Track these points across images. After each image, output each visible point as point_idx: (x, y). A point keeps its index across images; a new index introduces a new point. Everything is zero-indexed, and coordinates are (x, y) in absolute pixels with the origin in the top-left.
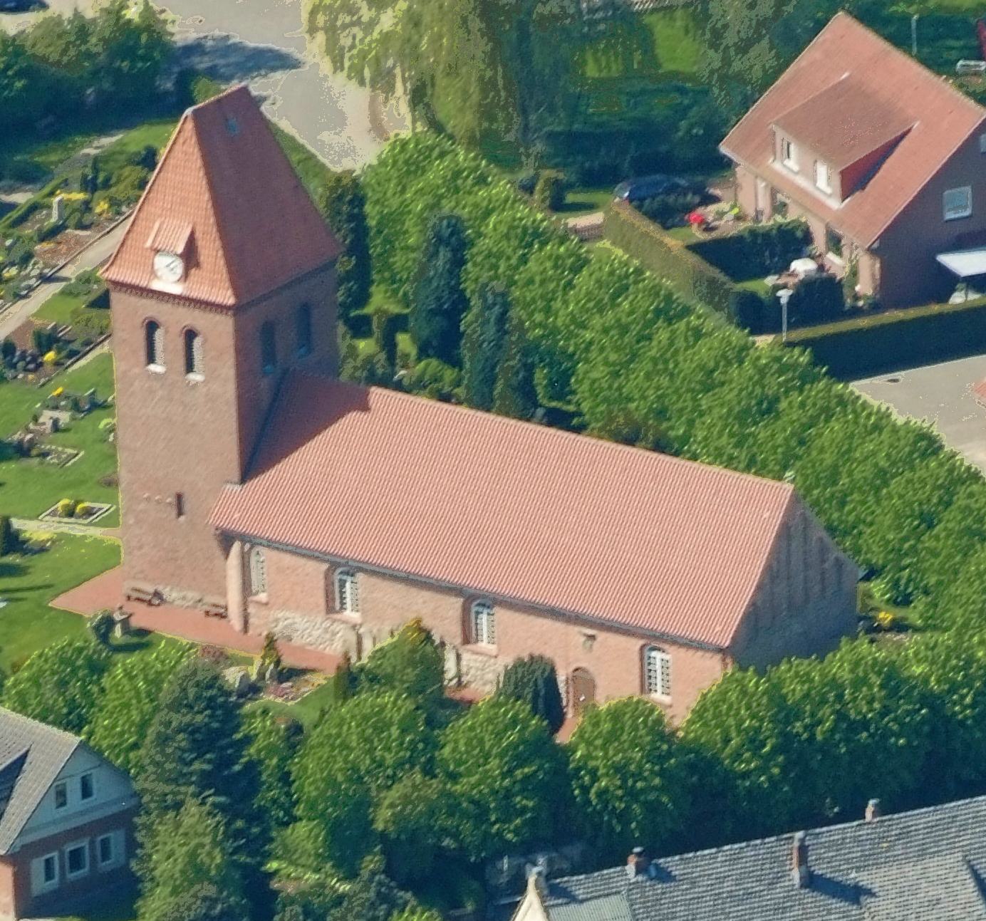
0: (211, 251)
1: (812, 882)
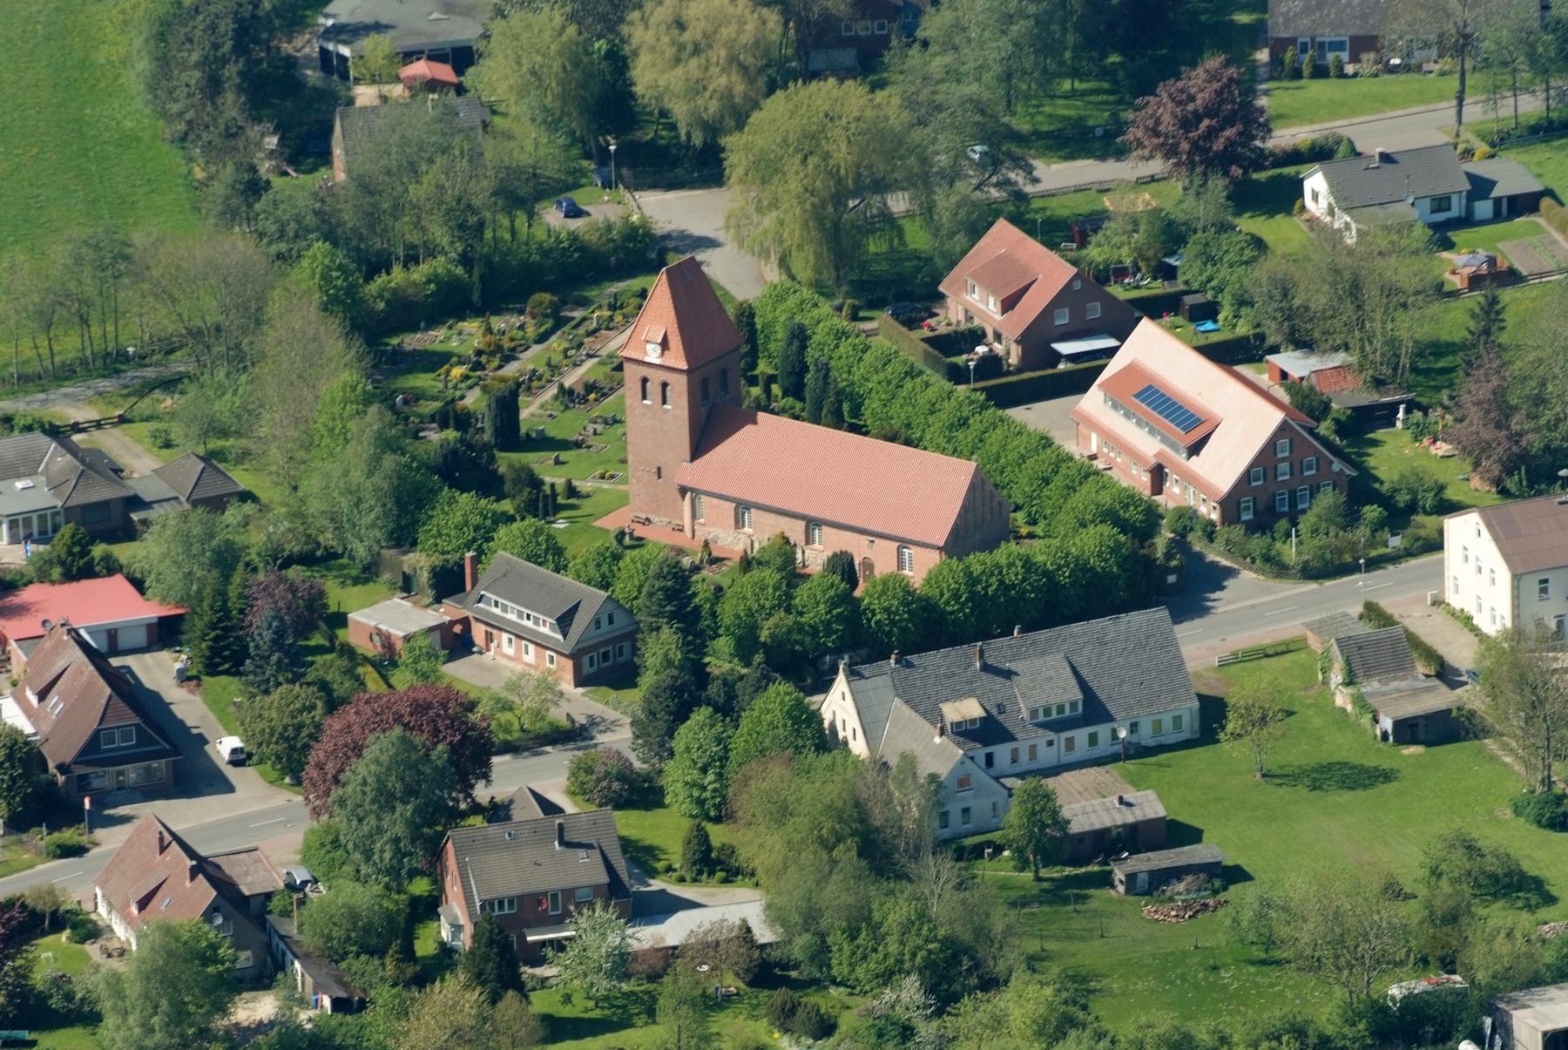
0: (676, 342)
1: (986, 668)
